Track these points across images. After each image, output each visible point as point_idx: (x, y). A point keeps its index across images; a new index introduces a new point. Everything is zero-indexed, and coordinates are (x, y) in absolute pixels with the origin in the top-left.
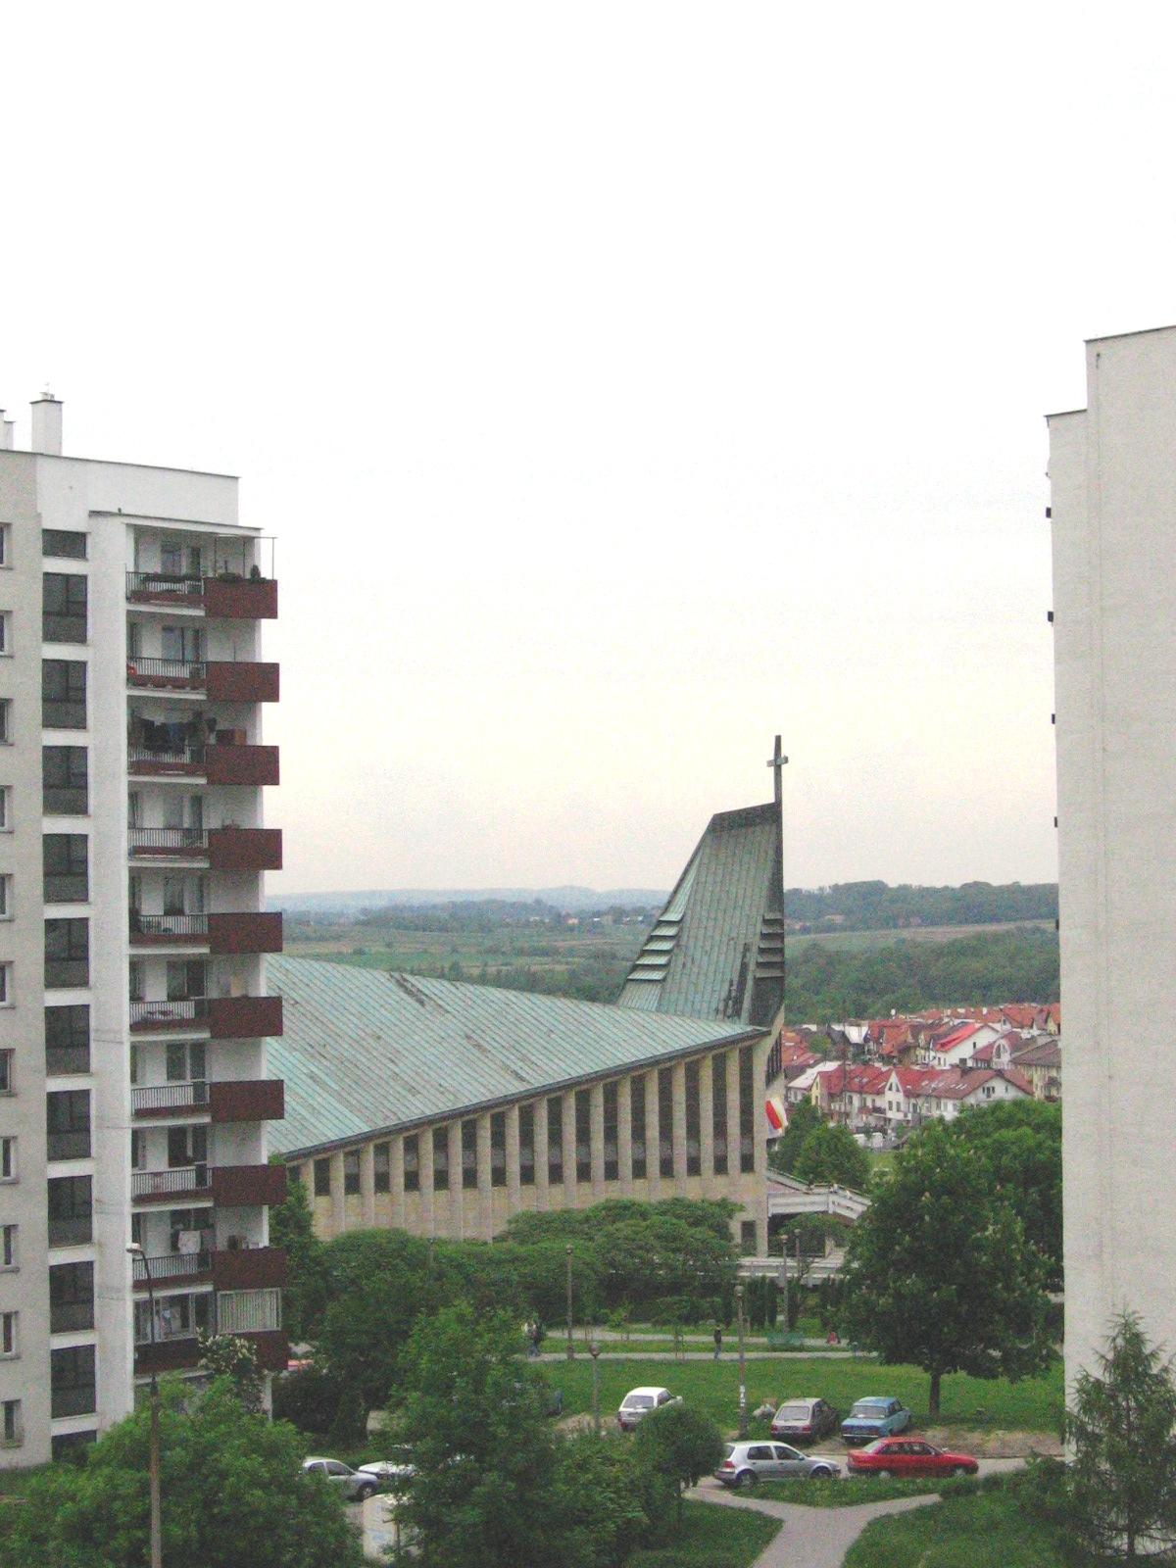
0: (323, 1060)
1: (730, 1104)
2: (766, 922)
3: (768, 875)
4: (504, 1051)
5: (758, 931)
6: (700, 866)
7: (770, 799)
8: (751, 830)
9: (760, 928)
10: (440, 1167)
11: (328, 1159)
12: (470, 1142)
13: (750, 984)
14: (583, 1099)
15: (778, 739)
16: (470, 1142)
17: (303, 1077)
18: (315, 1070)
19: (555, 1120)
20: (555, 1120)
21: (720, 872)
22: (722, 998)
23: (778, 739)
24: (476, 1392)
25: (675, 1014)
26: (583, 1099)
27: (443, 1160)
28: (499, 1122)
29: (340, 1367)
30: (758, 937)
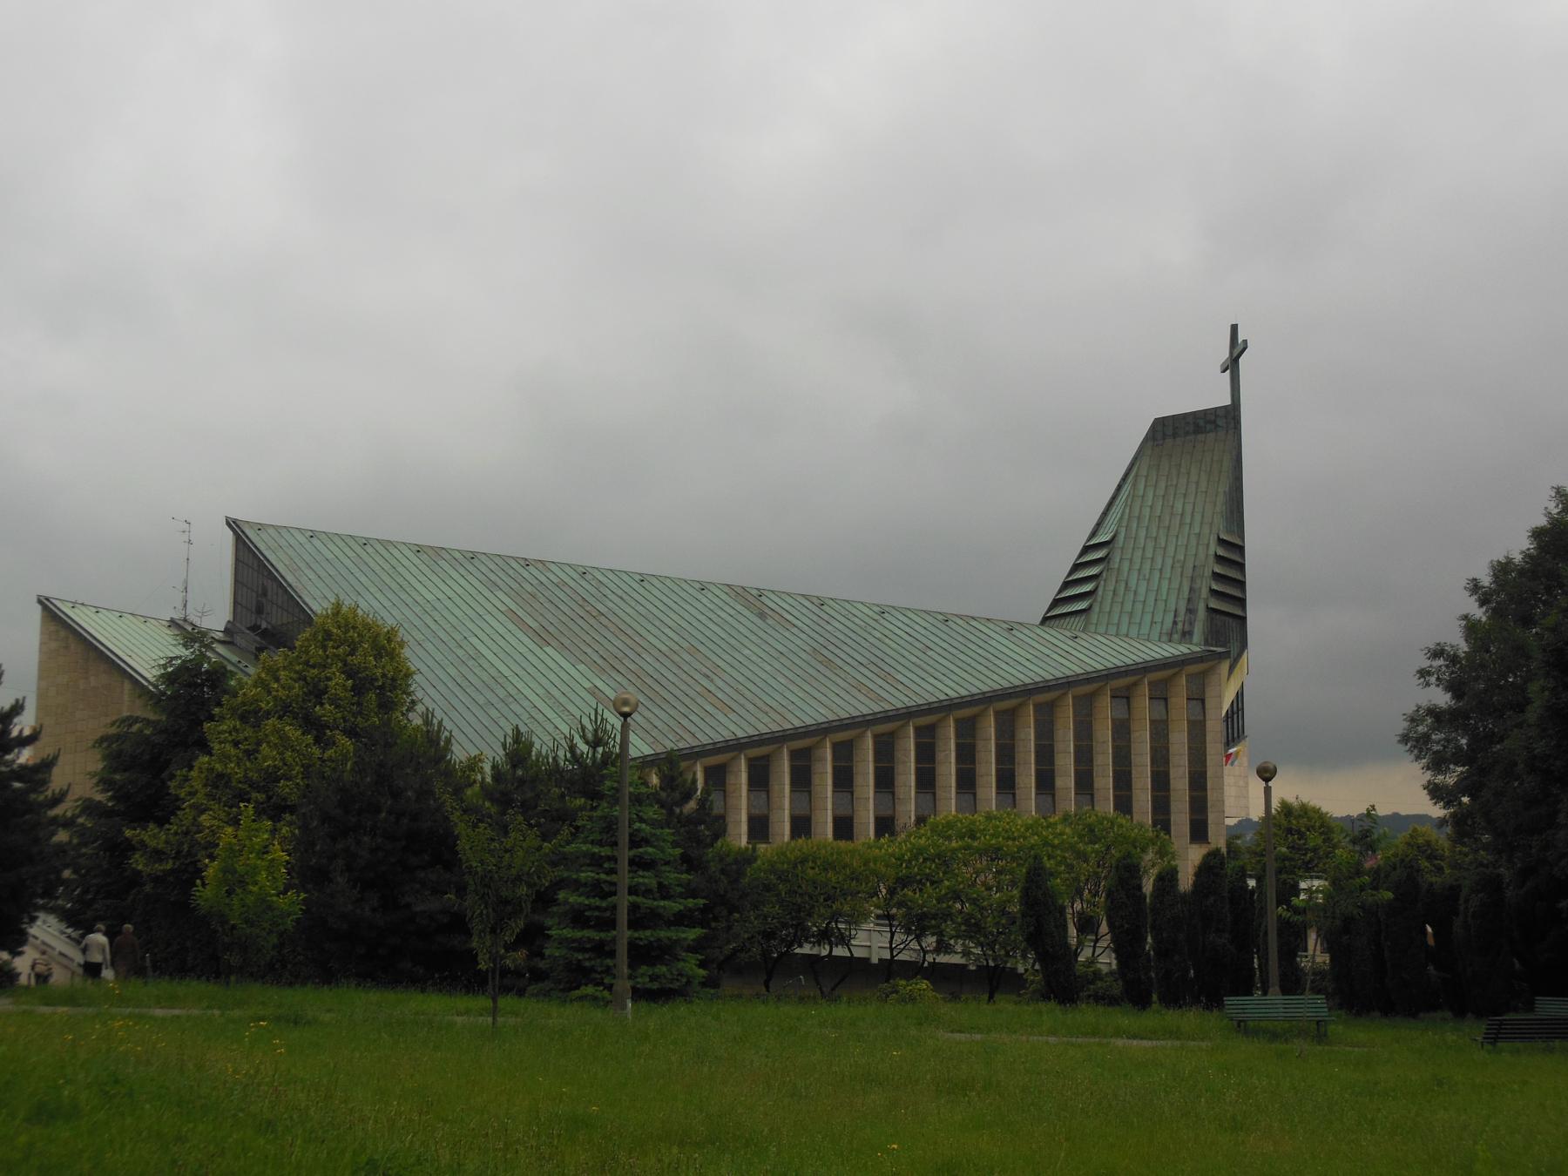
0: (614, 674)
1: (1173, 749)
2: (1222, 542)
3: (1224, 487)
4: (862, 669)
5: (1211, 552)
6: (1136, 476)
7: (1228, 402)
8: (1201, 437)
9: (1214, 548)
10: (756, 812)
11: (768, 756)
12: (802, 779)
13: (1202, 613)
14: (968, 730)
15: (1234, 328)
16: (802, 779)
17: (584, 694)
18: (599, 684)
19: (926, 754)
20: (926, 754)
21: (1162, 484)
22: (1164, 631)
23: (1234, 328)
24: (1521, 708)
25: (1117, 635)
26: (968, 730)
27: (1162, 707)
28: (886, 751)
29: (1127, 830)
30: (1212, 559)
